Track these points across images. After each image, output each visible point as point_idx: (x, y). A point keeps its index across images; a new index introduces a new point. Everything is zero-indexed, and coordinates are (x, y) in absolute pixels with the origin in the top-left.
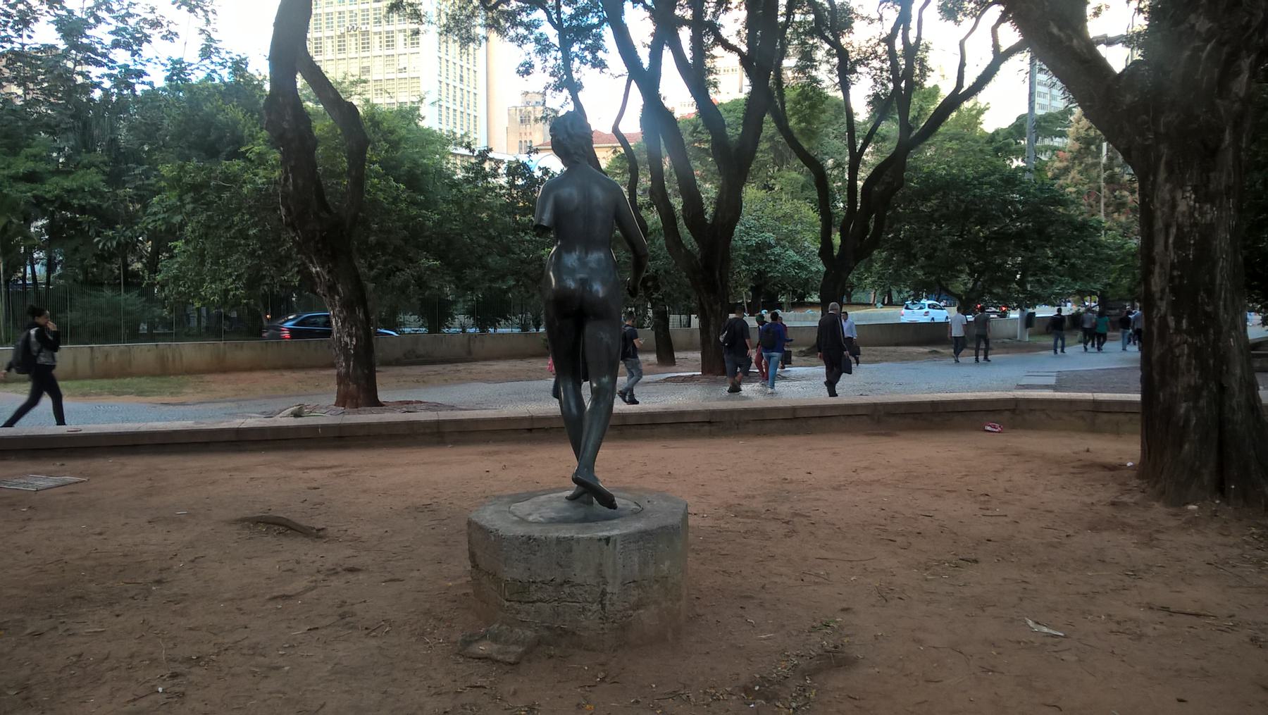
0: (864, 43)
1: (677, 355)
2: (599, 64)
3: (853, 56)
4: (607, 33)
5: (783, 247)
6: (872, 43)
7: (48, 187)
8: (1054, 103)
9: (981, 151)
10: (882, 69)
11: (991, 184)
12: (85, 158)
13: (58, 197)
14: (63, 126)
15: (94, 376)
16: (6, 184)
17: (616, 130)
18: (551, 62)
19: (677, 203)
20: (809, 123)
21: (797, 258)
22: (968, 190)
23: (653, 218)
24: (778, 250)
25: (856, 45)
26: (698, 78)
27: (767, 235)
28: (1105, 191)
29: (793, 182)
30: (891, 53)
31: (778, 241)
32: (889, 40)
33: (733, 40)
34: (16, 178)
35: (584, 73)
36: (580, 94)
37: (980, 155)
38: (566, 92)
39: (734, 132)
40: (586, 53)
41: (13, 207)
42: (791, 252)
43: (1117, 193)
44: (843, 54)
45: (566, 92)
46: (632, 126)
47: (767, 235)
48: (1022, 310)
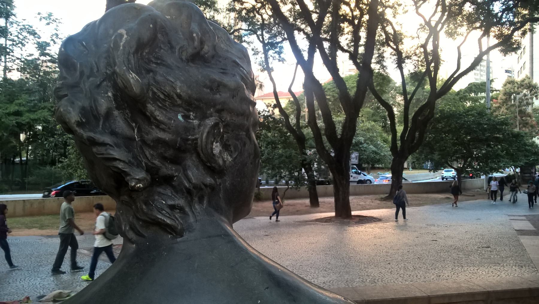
0: (409, 49)
1: (320, 200)
2: (282, 60)
3: (404, 55)
4: (286, 45)
5: (368, 144)
6: (413, 49)
7: (24, 118)
8: (482, 78)
9: (454, 99)
10: (418, 61)
11: (473, 115)
12: (42, 105)
13: (28, 123)
14: (34, 90)
15: (24, 215)
16: (4, 117)
17: (290, 91)
18: (259, 60)
19: (320, 123)
20: (381, 86)
21: (374, 149)
22: (461, 118)
23: (308, 132)
24: (365, 145)
25: (405, 50)
26: (331, 65)
27: (360, 138)
28: (519, 118)
29: (368, 113)
30: (425, 52)
31: (365, 140)
32: (424, 46)
33: (346, 48)
34: (9, 114)
35: (273, 63)
36: (272, 73)
37: (453, 101)
38: (266, 72)
39: (352, 93)
40: (276, 54)
41: (6, 128)
42: (371, 146)
43: (524, 118)
44: (399, 53)
45: (266, 72)
46: (299, 89)
47: (360, 138)
48: (486, 176)
